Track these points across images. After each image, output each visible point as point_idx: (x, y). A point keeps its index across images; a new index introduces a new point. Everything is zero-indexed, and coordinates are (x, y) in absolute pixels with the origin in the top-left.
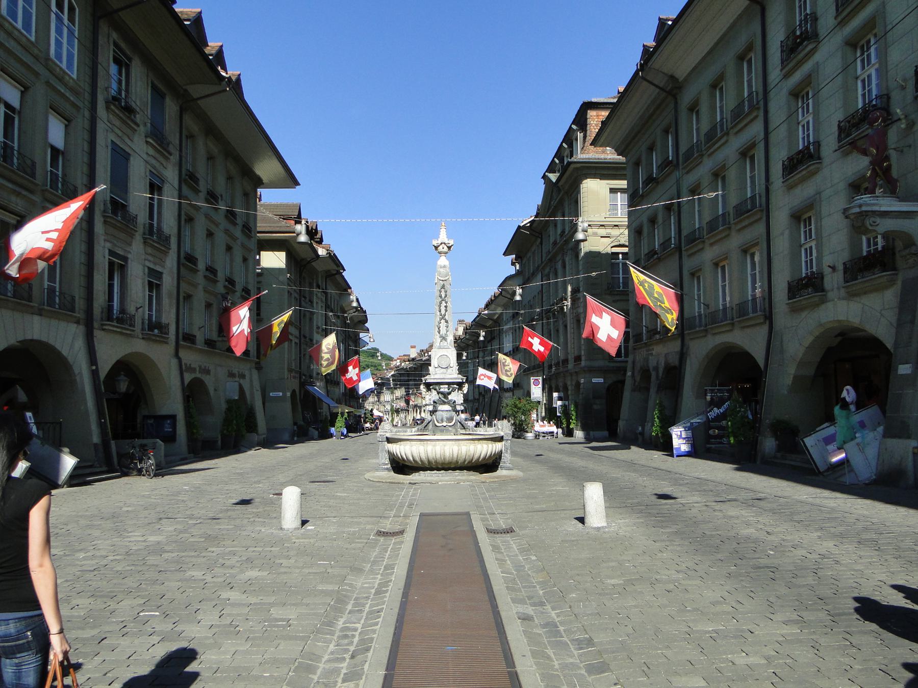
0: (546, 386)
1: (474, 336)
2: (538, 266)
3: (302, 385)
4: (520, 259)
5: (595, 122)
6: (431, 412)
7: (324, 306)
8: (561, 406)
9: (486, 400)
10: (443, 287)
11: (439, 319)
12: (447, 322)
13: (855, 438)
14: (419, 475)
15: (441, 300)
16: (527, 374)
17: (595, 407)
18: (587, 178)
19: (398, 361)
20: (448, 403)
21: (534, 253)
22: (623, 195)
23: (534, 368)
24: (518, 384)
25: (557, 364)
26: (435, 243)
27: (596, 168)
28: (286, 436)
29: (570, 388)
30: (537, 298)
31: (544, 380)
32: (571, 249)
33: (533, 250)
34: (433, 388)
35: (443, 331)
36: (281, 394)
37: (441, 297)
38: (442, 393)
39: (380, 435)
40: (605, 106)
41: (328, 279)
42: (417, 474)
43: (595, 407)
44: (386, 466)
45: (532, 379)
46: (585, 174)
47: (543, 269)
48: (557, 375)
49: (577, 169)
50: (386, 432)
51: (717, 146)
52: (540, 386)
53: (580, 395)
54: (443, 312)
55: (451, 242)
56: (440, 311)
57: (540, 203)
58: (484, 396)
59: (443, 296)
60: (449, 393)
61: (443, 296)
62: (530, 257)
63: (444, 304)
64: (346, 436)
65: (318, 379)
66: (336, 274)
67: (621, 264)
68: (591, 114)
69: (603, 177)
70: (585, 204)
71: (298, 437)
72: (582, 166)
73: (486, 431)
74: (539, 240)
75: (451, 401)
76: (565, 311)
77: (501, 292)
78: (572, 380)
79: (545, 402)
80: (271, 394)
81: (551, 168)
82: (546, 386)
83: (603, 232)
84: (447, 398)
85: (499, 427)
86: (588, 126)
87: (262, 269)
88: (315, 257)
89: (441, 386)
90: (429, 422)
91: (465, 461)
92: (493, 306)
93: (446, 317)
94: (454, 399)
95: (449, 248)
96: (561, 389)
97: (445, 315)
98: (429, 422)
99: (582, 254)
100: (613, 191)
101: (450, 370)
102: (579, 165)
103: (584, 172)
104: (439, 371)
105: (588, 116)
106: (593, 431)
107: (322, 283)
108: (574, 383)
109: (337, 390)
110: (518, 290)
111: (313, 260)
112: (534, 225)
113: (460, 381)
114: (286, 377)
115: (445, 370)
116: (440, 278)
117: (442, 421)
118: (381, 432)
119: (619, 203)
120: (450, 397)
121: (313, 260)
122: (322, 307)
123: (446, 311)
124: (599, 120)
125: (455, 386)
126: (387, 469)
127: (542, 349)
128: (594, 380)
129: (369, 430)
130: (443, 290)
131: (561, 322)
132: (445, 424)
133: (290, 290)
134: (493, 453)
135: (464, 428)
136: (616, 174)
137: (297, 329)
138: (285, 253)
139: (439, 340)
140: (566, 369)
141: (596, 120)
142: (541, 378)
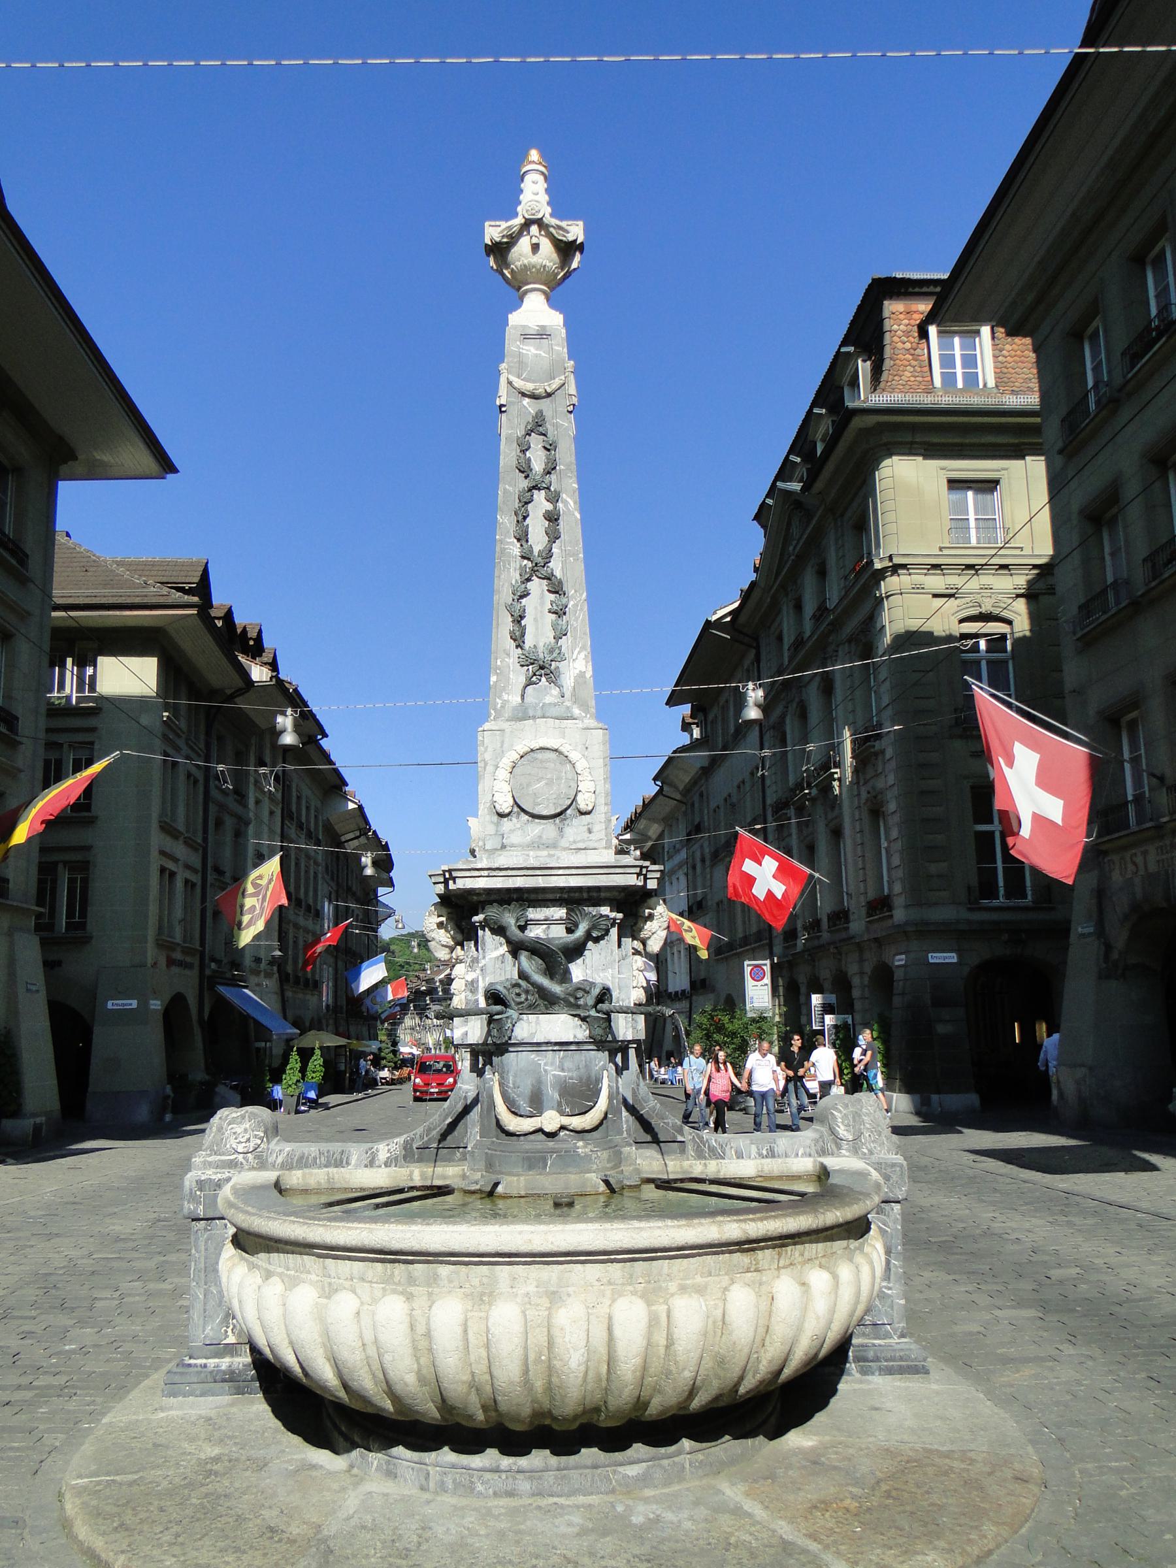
0: (781, 982)
3: (208, 983)
4: (701, 716)
5: (902, 327)
6: (476, 1051)
8: (836, 1027)
10: (537, 426)
11: (515, 577)
12: (557, 588)
14: (391, 1474)
15: (524, 484)
16: (726, 958)
17: (941, 1029)
18: (890, 455)
20: (572, 1003)
22: (980, 496)
23: (745, 941)
24: (703, 981)
25: (815, 925)
26: (493, 232)
27: (914, 428)
28: (143, 1113)
29: (856, 981)
31: (773, 966)
32: (774, 728)
34: (484, 925)
35: (539, 633)
36: (134, 1004)
37: (525, 470)
38: (537, 950)
39: (201, 1184)
40: (925, 289)
42: (376, 1458)
43: (941, 1029)
44: (225, 1363)
45: (748, 966)
46: (885, 444)
48: (813, 953)
49: (866, 432)
50: (233, 1164)
52: (767, 980)
54: (538, 539)
55: (575, 231)
56: (522, 537)
59: (538, 466)
60: (575, 951)
61: (538, 466)
62: (727, 701)
63: (540, 502)
64: (314, 1104)
65: (257, 973)
67: (984, 663)
68: (893, 308)
69: (931, 451)
70: (890, 517)
71: (174, 1112)
72: (878, 423)
73: (772, 1154)
75: (584, 988)
76: (837, 792)
77: (661, 788)
79: (777, 1019)
80: (110, 1005)
81: (785, 472)
82: (781, 982)
83: (937, 582)
84: (565, 977)
85: (842, 1131)
86: (887, 336)
87: (102, 698)
89: (533, 914)
90: (467, 1110)
91: (692, 1393)
92: (642, 824)
93: (556, 566)
94: (603, 978)
95: (566, 249)
96: (827, 985)
97: (548, 555)
98: (467, 1110)
99: (888, 639)
100: (955, 484)
101: (575, 829)
102: (872, 420)
103: (885, 440)
104: (519, 831)
105: (886, 314)
106: (938, 1092)
108: (868, 968)
109: (312, 1000)
110: (751, 693)
112: (742, 619)
113: (632, 880)
114: (150, 962)
115: (547, 829)
116: (518, 383)
117: (537, 1104)
118: (207, 1165)
119: (972, 517)
120: (578, 971)
122: (272, 813)
123: (553, 536)
124: (913, 322)
125: (605, 910)
126: (231, 1378)
127: (779, 890)
128: (935, 958)
129: (387, 1083)
130: (536, 441)
132: (551, 1120)
133: (194, 770)
135: (656, 1141)
136: (961, 445)
137: (196, 850)
138: (155, 660)
139: (518, 676)
140: (844, 935)
141: (906, 322)
142: (768, 962)
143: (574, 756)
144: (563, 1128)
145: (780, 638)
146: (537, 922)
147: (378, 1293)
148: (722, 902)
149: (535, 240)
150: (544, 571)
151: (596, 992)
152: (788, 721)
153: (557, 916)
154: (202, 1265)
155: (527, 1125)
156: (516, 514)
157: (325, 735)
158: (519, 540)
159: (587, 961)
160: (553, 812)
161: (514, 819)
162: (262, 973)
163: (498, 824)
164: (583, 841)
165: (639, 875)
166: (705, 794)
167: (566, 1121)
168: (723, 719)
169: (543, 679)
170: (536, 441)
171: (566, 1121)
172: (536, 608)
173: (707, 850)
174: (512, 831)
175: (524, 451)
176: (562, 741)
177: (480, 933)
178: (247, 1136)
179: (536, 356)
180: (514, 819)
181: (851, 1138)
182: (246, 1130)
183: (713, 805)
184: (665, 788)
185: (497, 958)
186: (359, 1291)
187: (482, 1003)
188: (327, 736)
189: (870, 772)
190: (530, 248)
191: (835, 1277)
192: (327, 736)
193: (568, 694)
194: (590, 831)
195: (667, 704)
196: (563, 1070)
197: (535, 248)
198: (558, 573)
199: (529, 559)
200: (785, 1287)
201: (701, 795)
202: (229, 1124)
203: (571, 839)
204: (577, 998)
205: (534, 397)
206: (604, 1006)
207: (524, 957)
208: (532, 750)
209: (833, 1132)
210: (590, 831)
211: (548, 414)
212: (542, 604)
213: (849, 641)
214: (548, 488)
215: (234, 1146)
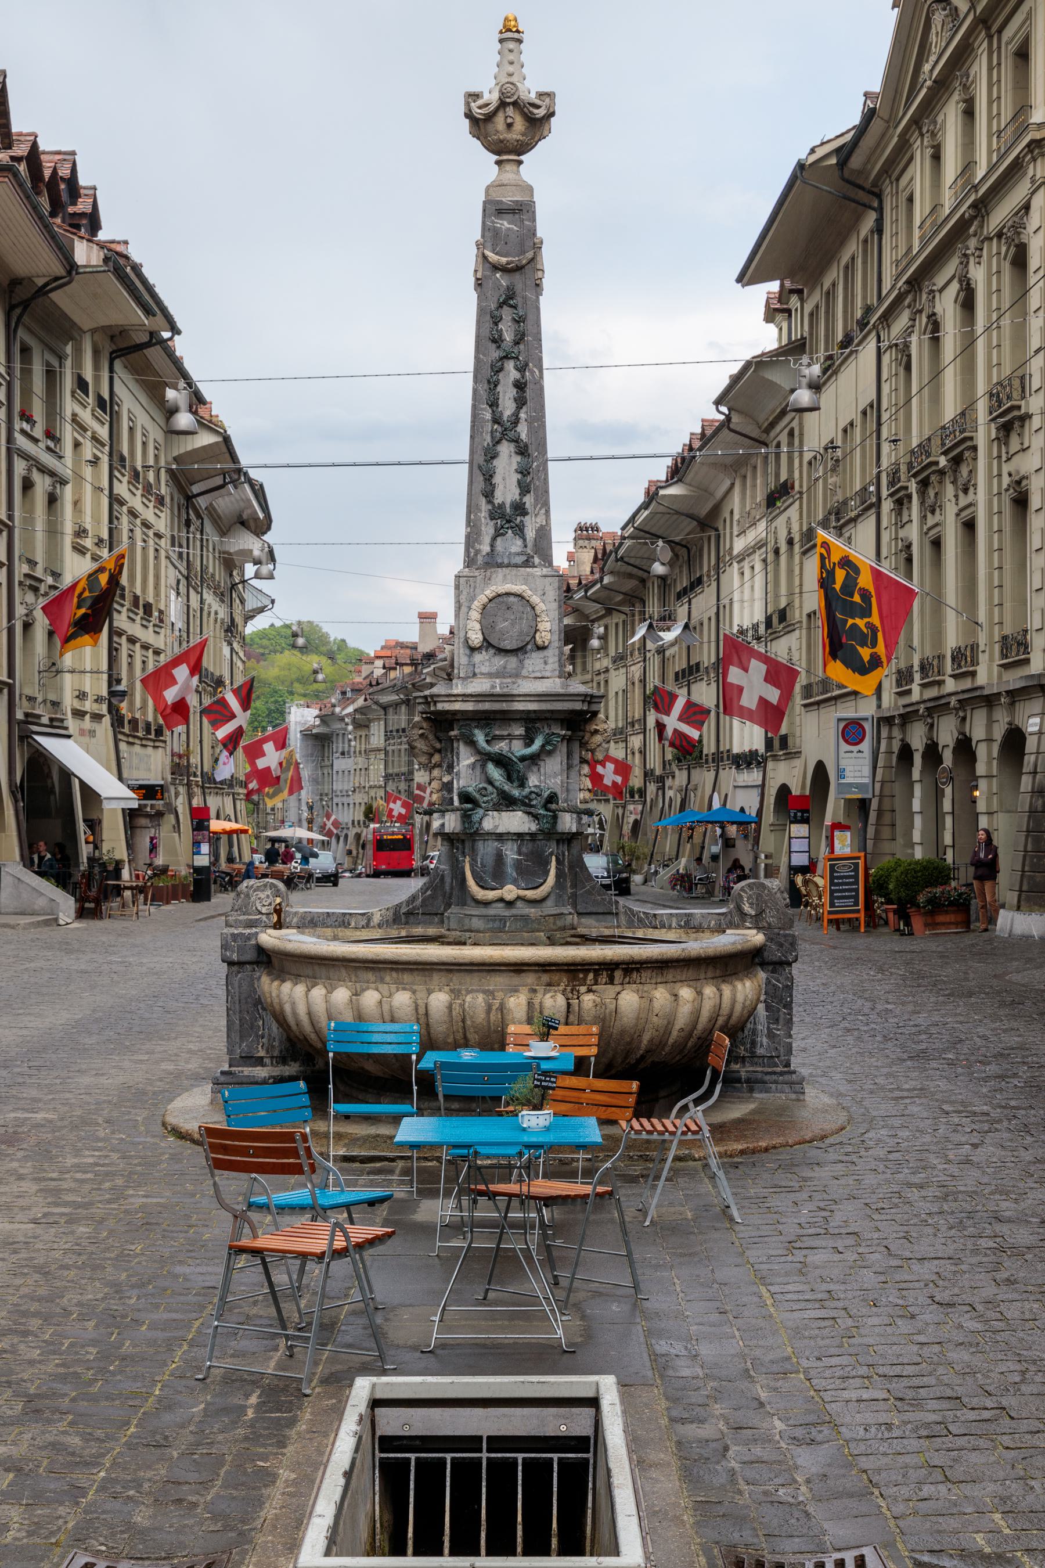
1: (630, 576)
2: (868, 310)
7: (105, 459)
9: (670, 793)
12: (523, 451)
13: (27, 715)
15: (496, 354)
16: (818, 703)
19: (379, 663)
20: (524, 804)
21: (849, 268)
29: (981, 751)
30: (858, 430)
33: (845, 258)
38: (501, 761)
41: (118, 365)
47: (887, 318)
51: (620, 708)
53: (1024, 778)
54: (507, 407)
57: (876, 86)
58: (661, 780)
59: (508, 337)
61: (508, 337)
62: (853, 258)
63: (511, 372)
66: (148, 345)
74: (871, 217)
77: (728, 418)
78: (990, 722)
85: (747, 908)
88: (61, 272)
97: (516, 422)
101: (533, 662)
104: (484, 661)
107: (97, 378)
108: (999, 732)
111: (56, 283)
115: (512, 662)
121: (56, 283)
130: (507, 313)
131: (951, 510)
132: (510, 891)
134: (705, 1014)
143: (535, 599)
144: (519, 898)
145: (910, 200)
146: (502, 738)
147: (393, 990)
148: (815, 613)
149: (509, 120)
150: (511, 434)
151: (546, 794)
152: (914, 339)
153: (517, 733)
154: (237, 998)
155: (491, 895)
156: (489, 382)
157: (175, 330)
158: (490, 406)
159: (542, 770)
160: (515, 647)
161: (484, 652)
162: (88, 717)
163: (470, 656)
164: (540, 671)
165: (583, 701)
166: (796, 433)
167: (522, 893)
168: (827, 312)
169: (510, 531)
170: (507, 313)
171: (522, 893)
172: (504, 468)
173: (795, 527)
174: (482, 662)
175: (496, 324)
176: (524, 587)
177: (455, 745)
178: (269, 901)
179: (509, 229)
180: (484, 652)
181: (753, 913)
182: (268, 896)
183: (807, 456)
184: (735, 419)
185: (468, 766)
186: (380, 989)
187: (456, 803)
188: (179, 333)
189: (1014, 444)
190: (505, 126)
191: (700, 993)
192: (179, 333)
193: (530, 544)
194: (546, 663)
195: (739, 280)
196: (520, 854)
197: (509, 126)
198: (523, 436)
199: (499, 423)
200: (661, 995)
201: (791, 434)
202: (255, 891)
203: (530, 669)
204: (530, 800)
205: (504, 269)
206: (553, 806)
207: (490, 766)
208: (499, 595)
209: (739, 909)
210: (546, 663)
211: (519, 287)
212: (511, 463)
213: (1000, 235)
214: (517, 358)
215: (259, 908)
